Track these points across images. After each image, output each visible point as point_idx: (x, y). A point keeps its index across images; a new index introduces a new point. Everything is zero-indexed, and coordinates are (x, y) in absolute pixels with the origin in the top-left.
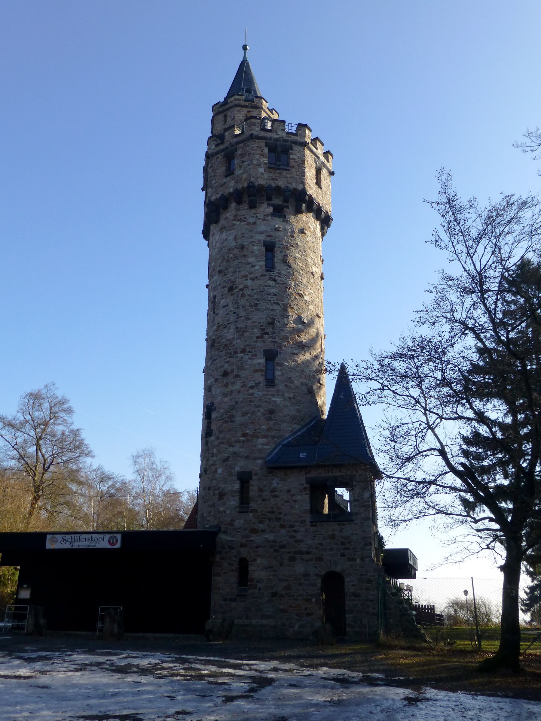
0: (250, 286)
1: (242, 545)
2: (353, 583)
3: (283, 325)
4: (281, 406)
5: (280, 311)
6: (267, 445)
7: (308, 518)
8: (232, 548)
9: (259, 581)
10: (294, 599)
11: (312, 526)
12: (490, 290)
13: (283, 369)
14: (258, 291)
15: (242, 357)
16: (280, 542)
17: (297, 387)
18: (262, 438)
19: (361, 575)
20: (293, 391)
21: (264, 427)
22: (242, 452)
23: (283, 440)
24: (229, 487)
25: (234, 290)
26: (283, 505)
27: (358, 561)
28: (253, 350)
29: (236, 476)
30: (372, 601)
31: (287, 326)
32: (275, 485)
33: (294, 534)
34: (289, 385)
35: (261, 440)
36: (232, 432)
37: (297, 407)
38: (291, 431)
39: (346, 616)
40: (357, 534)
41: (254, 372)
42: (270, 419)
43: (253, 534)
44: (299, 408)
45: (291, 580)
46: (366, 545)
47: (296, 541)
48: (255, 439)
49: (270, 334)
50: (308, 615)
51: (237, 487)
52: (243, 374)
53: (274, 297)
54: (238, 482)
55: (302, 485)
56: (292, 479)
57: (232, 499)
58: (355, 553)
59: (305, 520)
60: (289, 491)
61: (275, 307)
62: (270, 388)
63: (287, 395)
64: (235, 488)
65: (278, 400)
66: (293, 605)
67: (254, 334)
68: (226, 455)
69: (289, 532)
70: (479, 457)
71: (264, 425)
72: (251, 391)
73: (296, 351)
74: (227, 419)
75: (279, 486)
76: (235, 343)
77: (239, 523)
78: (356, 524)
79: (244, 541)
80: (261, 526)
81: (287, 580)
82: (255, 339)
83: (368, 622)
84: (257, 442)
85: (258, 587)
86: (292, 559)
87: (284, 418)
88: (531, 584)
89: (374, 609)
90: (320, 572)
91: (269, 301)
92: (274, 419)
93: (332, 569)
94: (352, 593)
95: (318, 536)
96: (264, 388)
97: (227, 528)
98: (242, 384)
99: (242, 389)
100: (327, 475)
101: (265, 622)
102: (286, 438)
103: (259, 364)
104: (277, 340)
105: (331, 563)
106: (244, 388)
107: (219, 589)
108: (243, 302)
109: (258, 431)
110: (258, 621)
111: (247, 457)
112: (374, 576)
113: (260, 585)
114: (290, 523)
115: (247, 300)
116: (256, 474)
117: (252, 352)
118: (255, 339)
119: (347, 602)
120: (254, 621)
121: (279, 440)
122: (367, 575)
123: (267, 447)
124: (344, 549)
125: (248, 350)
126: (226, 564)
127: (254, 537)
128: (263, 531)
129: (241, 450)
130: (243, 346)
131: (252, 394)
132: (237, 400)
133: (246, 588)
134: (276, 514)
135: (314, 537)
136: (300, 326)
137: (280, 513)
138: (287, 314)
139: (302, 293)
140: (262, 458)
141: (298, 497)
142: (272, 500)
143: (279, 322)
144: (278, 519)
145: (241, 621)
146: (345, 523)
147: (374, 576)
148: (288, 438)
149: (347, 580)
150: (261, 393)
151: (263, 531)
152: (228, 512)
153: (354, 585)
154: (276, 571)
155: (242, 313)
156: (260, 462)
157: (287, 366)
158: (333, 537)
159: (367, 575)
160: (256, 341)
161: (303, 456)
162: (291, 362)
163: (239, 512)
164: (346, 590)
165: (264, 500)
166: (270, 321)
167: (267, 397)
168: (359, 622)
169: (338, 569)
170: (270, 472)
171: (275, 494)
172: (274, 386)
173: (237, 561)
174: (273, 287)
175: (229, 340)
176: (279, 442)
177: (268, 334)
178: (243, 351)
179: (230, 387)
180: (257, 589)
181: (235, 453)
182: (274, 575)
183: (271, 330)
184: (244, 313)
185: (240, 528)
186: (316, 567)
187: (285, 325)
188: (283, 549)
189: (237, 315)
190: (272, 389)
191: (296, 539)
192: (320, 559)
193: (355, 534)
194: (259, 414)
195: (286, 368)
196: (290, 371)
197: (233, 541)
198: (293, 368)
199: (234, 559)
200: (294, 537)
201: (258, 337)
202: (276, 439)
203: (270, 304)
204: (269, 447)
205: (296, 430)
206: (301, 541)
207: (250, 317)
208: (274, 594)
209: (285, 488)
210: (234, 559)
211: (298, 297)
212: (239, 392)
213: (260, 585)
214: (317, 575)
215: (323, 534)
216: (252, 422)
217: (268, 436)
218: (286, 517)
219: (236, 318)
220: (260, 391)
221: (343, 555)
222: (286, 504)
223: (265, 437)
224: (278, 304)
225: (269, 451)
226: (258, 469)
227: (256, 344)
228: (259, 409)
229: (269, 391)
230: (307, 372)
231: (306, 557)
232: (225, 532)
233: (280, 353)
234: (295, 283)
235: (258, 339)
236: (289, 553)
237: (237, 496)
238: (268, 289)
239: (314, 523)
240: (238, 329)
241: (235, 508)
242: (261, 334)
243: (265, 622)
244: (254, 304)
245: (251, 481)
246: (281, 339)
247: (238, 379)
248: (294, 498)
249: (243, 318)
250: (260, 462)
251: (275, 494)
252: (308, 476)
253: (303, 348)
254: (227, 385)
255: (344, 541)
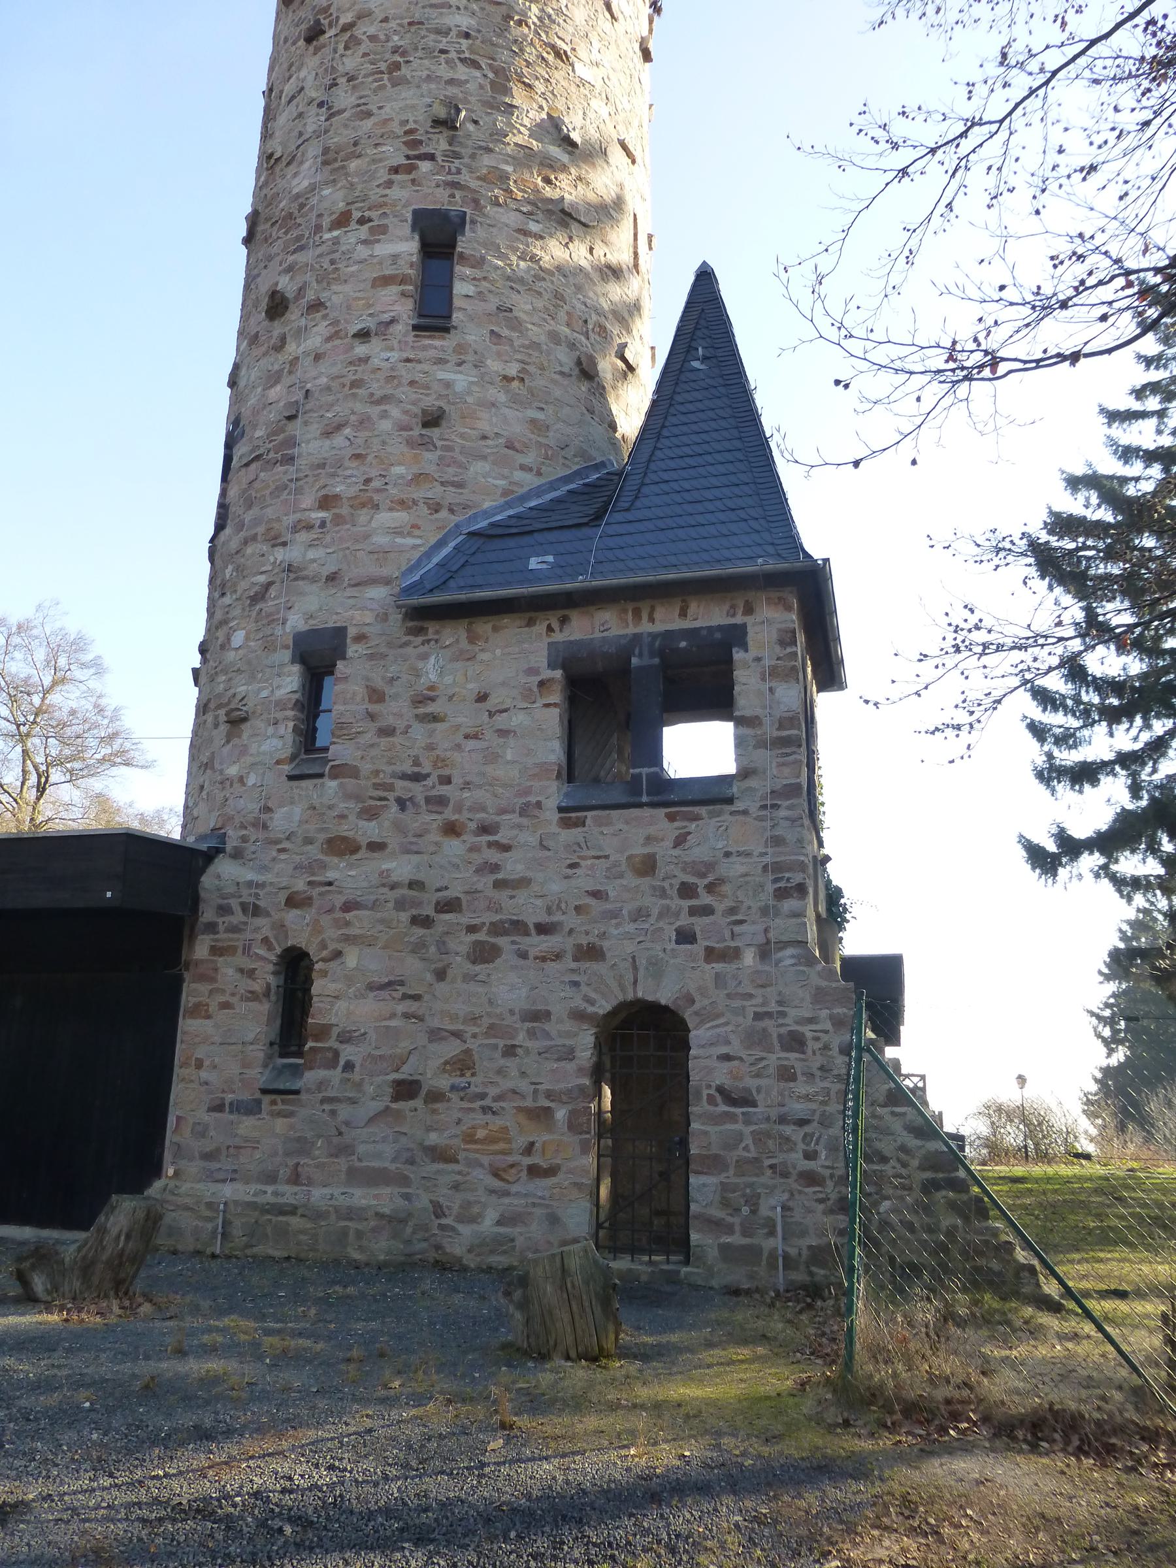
0: (377, 11)
1: (293, 901)
2: (724, 1050)
3: (491, 135)
4: (470, 400)
5: (481, 87)
6: (409, 534)
7: (552, 794)
8: (256, 911)
9: (346, 1038)
10: (485, 1110)
11: (566, 824)
12: (556, 1401)
13: (485, 278)
14: (406, 21)
15: (336, 241)
16: (438, 890)
17: (535, 345)
18: (391, 509)
19: (758, 1016)
20: (519, 357)
21: (398, 470)
22: (314, 561)
23: (474, 517)
24: (264, 688)
25: (324, 32)
26: (458, 747)
27: (749, 958)
28: (374, 214)
29: (286, 647)
30: (802, 1123)
31: (507, 140)
32: (433, 677)
33: (494, 856)
34: (505, 332)
35: (385, 518)
36: (284, 496)
37: (532, 413)
38: (505, 493)
39: (691, 1180)
40: (748, 854)
41: (373, 286)
42: (425, 444)
43: (336, 860)
44: (540, 416)
45: (474, 1036)
46: (782, 894)
47: (499, 885)
48: (363, 516)
49: (439, 159)
50: (534, 1171)
51: (289, 689)
52: (336, 296)
53: (463, 41)
54: (296, 668)
55: (532, 671)
56: (498, 652)
57: (270, 730)
58: (737, 929)
59: (539, 805)
60: (482, 698)
61: (462, 72)
62: (430, 337)
63: (494, 366)
64: (280, 693)
65: (461, 380)
66: (481, 1134)
67: (381, 160)
68: (262, 579)
69: (473, 849)
70: (1067, 739)
71: (400, 464)
72: (361, 350)
73: (533, 227)
74: (272, 455)
75: (448, 680)
76: (314, 201)
77: (286, 818)
78: (745, 812)
79: (300, 885)
80: (370, 830)
81: (457, 1034)
82: (386, 177)
83: (785, 1208)
84: (374, 524)
85: (342, 1063)
86: (484, 954)
87: (483, 443)
88: (1104, 1063)
89: (810, 1156)
90: (592, 1002)
91: (442, 51)
92: (439, 443)
93: (640, 995)
94: (720, 1090)
95: (589, 862)
96: (410, 338)
97: (244, 839)
98: (332, 330)
99: (329, 345)
100: (631, 630)
101: (361, 1197)
102: (486, 514)
103: (395, 257)
104: (465, 178)
105: (635, 968)
106: (337, 342)
107: (199, 1065)
108: (350, 63)
109: (376, 484)
110: (337, 1192)
111: (332, 578)
112: (811, 1021)
113: (348, 1052)
114: (483, 815)
115: (365, 55)
116: (360, 638)
117: (370, 220)
118: (383, 175)
119: (695, 1126)
120: (318, 1195)
121: (455, 519)
122: (783, 1014)
123: (410, 541)
124: (693, 911)
125: (356, 215)
126: (230, 972)
127: (338, 870)
128: (376, 847)
129: (311, 554)
130: (341, 204)
131: (366, 360)
132: (309, 386)
133: (301, 1061)
134: (429, 782)
135: (573, 866)
136: (555, 151)
137: (446, 780)
138: (507, 100)
139: (567, 48)
140: (387, 582)
141: (517, 720)
142: (419, 732)
143: (476, 122)
144: (441, 802)
145: (270, 1189)
146: (696, 809)
147: (811, 1021)
148: (494, 515)
149: (698, 1035)
150: (395, 356)
151: (376, 847)
152: (251, 780)
153: (727, 1058)
154: (416, 998)
155: (344, 98)
156: (378, 593)
157: (497, 268)
158: (647, 867)
159: (783, 1014)
160: (389, 184)
161: (539, 566)
162: (514, 258)
163: (291, 778)
164: (694, 1077)
165: (387, 732)
166: (442, 113)
167: (419, 367)
168: (745, 1210)
169: (664, 996)
170: (420, 631)
171: (431, 708)
172: (447, 330)
173: (273, 958)
174: (458, 8)
175: (298, 196)
176: (457, 526)
177: (431, 157)
178: (342, 221)
179: (292, 348)
180: (340, 1069)
181: (290, 568)
182: (406, 1016)
183: (444, 145)
184: (353, 99)
185: (288, 839)
186: (576, 984)
187: (499, 136)
188: (447, 917)
189: (329, 108)
190: (437, 343)
191: (500, 876)
192: (592, 953)
193: (739, 854)
194: (386, 425)
195: (493, 275)
196: (512, 288)
197: (262, 885)
198: (521, 281)
199: (261, 952)
200: (495, 868)
201: (395, 170)
202: (444, 514)
203: (447, 63)
204: (418, 541)
205: (526, 489)
206: (523, 882)
207: (373, 108)
208: (406, 1090)
209: (470, 686)
210: (261, 952)
211: (551, 58)
212: (318, 357)
213: (348, 1052)
214: (579, 1016)
215: (607, 857)
216: (357, 456)
217: (415, 503)
218: (466, 794)
219: (323, 118)
220: (392, 349)
221: (685, 937)
222: (471, 744)
223: (402, 504)
224: (475, 65)
225: (416, 555)
226: (369, 618)
227: (388, 191)
228: (387, 407)
229: (425, 348)
230: (579, 306)
231: (539, 944)
232: (237, 855)
233: (473, 222)
234: (542, 10)
235: (394, 177)
236: (472, 929)
237: (286, 718)
238: (441, 14)
239: (573, 815)
240: (328, 158)
241: (278, 762)
242: (408, 157)
243: (361, 1197)
244: (388, 67)
245: (340, 665)
246: (479, 178)
247: (319, 315)
248: (501, 720)
249: (346, 115)
250: (378, 593)
251: (431, 708)
252: (558, 637)
253: (564, 225)
254: (280, 346)
255: (692, 879)
